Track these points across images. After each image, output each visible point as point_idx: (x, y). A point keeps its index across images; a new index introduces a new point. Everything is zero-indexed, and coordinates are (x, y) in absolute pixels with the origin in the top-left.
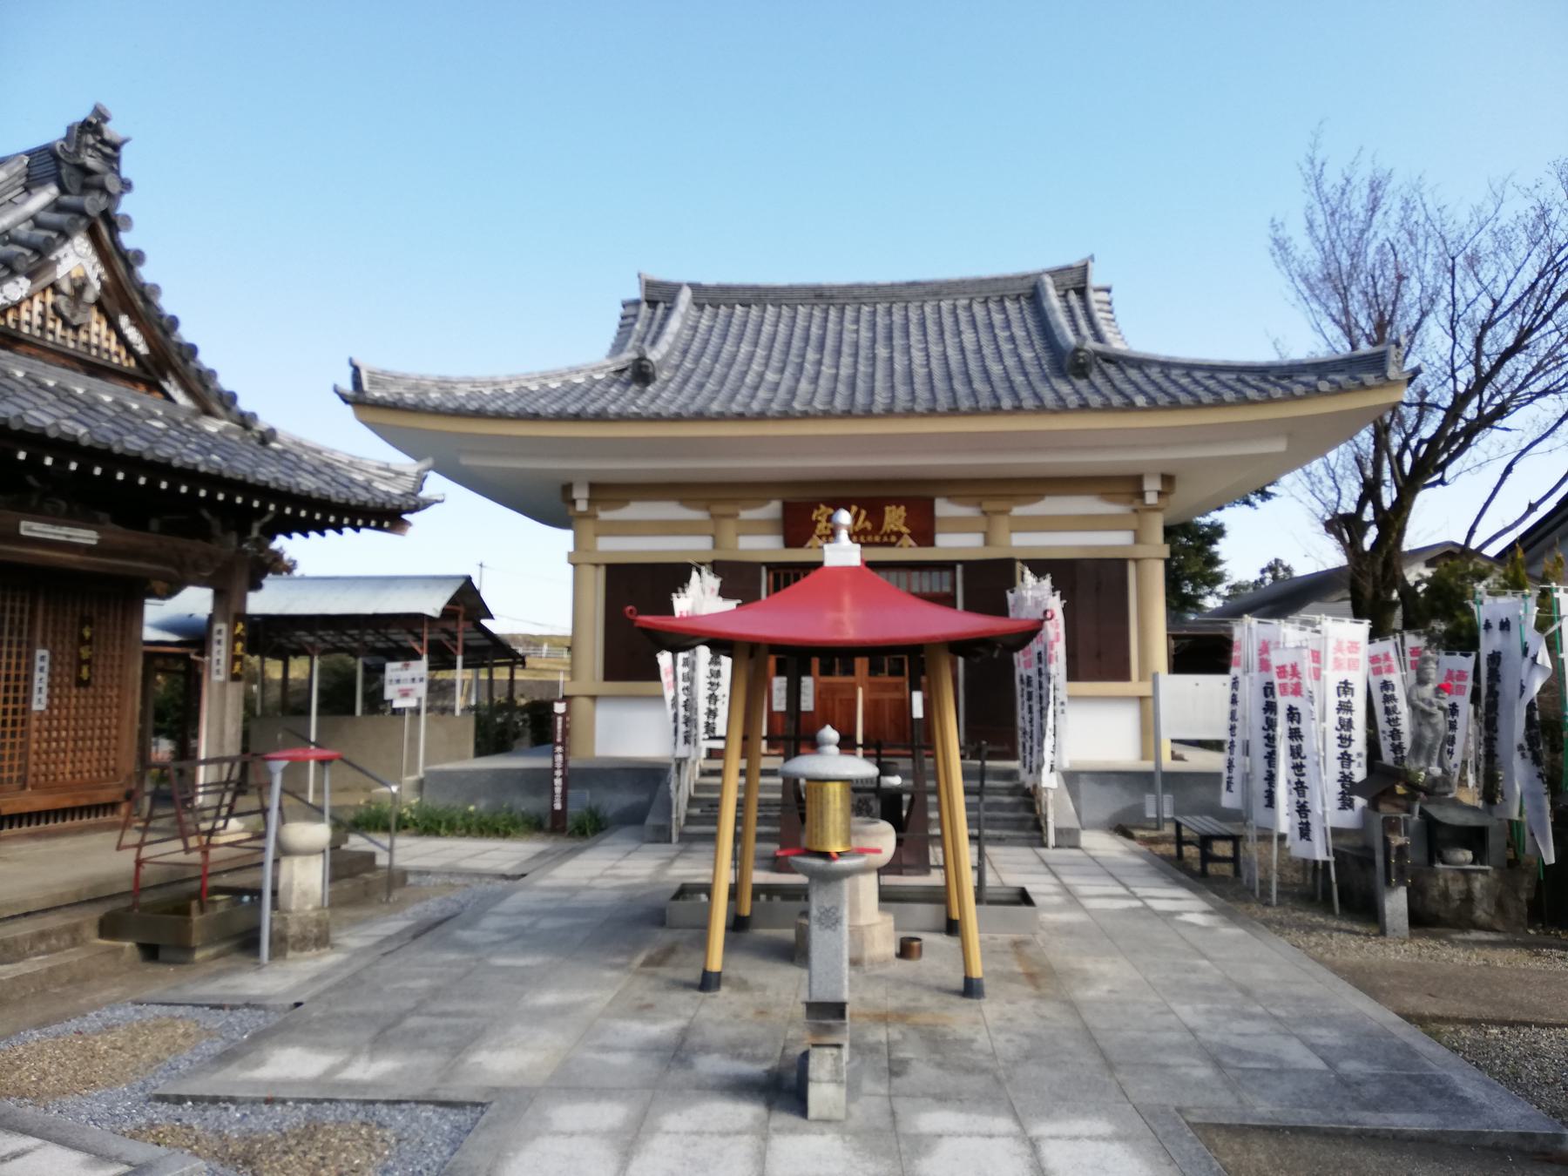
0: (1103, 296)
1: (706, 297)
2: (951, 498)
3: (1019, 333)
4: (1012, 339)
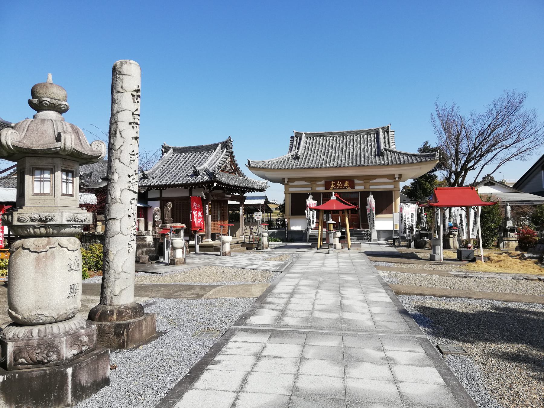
0: (393, 133)
1: (308, 135)
2: (358, 179)
3: (373, 143)
4: (371, 145)
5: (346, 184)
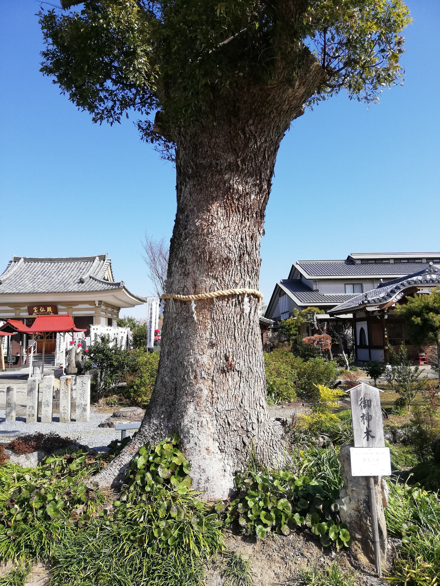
5: (49, 309)
